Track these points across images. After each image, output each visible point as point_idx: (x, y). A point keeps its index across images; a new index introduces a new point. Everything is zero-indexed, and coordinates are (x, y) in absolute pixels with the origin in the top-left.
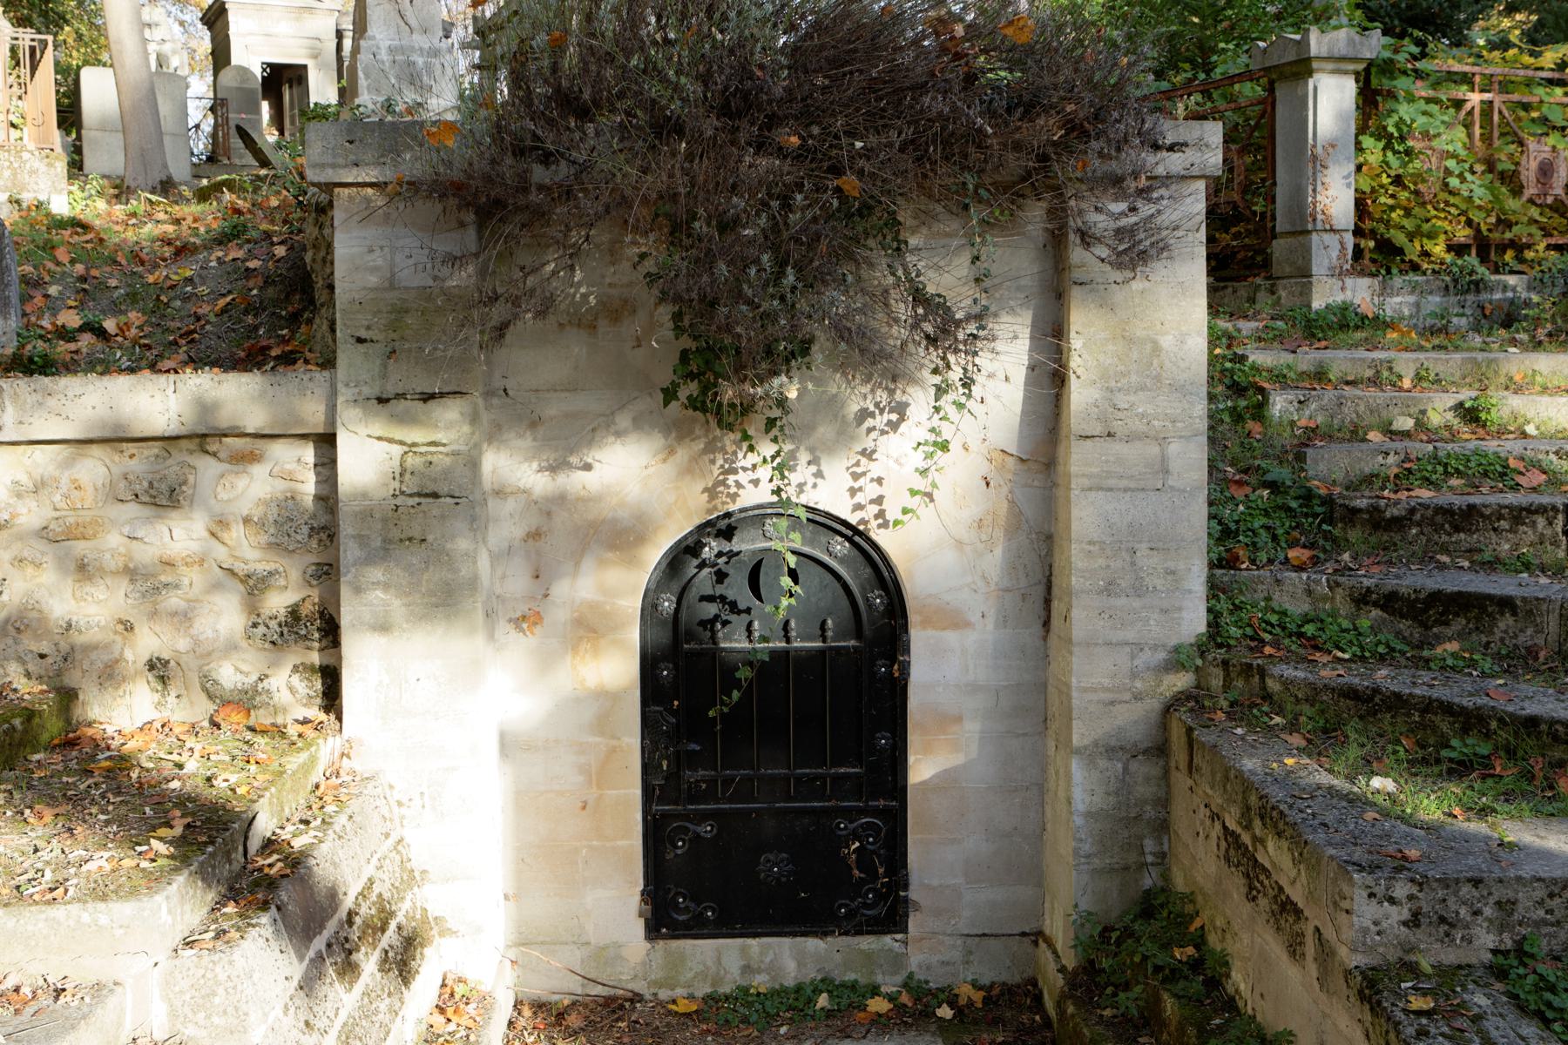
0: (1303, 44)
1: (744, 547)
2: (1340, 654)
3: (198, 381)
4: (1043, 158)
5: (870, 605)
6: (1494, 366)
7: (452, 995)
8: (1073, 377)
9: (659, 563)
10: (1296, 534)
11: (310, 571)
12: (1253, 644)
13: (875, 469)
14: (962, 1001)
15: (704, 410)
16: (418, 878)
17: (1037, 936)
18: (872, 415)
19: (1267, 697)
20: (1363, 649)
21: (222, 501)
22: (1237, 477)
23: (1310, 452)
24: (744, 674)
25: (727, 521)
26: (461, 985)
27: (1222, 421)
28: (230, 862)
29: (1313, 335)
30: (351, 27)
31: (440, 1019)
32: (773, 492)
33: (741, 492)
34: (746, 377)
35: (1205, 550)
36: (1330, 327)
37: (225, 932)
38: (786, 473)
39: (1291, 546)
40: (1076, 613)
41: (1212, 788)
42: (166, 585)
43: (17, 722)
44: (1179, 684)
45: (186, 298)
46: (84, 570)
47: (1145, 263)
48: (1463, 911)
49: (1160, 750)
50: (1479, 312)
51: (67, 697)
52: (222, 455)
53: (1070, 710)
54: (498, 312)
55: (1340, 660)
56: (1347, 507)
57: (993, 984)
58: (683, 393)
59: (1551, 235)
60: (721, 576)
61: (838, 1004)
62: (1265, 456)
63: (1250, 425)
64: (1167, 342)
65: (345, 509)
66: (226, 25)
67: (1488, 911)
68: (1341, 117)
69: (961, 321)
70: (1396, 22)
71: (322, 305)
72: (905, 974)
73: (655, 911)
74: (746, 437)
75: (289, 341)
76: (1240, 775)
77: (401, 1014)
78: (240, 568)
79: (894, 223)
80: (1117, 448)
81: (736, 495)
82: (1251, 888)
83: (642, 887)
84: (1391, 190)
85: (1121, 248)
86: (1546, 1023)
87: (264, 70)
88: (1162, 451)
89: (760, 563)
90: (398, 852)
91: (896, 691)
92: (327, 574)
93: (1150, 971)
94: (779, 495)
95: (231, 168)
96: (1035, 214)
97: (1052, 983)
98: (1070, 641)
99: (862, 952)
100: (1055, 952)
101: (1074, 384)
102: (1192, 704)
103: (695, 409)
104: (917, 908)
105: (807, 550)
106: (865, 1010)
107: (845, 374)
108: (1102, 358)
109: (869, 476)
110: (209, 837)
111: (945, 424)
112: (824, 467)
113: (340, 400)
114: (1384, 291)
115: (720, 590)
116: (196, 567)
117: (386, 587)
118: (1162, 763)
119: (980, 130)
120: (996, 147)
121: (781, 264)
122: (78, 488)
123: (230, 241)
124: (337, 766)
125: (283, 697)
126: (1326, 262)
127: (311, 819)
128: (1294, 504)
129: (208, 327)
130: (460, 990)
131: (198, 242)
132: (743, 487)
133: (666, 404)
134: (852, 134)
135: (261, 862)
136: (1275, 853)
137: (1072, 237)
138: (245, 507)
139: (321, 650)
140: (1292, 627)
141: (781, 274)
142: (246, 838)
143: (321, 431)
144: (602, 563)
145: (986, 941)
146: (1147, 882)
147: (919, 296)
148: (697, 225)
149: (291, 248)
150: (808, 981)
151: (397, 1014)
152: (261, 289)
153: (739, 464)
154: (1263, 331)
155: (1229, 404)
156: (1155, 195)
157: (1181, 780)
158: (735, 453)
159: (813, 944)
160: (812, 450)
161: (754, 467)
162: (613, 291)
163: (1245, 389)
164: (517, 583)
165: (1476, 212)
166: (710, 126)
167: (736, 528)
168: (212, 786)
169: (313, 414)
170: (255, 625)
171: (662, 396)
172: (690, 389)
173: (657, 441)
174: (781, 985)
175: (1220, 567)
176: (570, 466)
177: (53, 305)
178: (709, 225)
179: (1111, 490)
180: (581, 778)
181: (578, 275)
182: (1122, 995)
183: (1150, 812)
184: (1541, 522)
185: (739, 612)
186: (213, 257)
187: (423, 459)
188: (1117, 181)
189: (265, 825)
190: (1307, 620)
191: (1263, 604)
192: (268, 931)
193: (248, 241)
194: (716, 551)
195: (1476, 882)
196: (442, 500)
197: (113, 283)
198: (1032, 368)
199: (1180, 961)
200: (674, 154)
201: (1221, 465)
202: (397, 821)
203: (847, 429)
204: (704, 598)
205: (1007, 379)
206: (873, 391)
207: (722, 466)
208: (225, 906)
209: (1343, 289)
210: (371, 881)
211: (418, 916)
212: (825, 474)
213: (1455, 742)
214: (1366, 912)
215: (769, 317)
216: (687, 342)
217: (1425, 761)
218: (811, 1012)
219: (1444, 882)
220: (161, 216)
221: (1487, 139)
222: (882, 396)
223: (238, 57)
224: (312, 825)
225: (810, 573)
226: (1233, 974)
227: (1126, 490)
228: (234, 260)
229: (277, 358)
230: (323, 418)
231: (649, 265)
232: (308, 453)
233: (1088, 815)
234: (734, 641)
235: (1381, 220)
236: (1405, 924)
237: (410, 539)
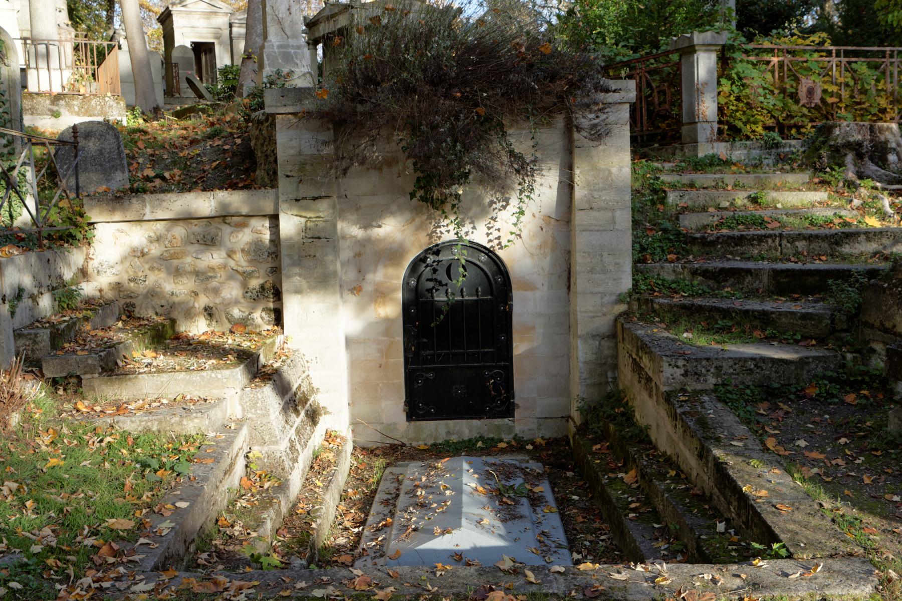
0: (691, 39)
1: (444, 258)
2: (684, 294)
3: (223, 194)
6: (768, 180)
8: (576, 185)
10: (672, 249)
13: (497, 225)
17: (568, 418)
18: (495, 203)
19: (654, 311)
20: (693, 292)
23: (681, 216)
29: (697, 169)
31: (327, 443)
36: (705, 165)
39: (669, 254)
40: (578, 281)
42: (211, 277)
43: (160, 327)
45: (198, 163)
46: (177, 273)
48: (703, 370)
49: (613, 336)
50: (778, 157)
51: (173, 322)
52: (232, 224)
54: (344, 164)
55: (683, 296)
56: (692, 237)
57: (550, 438)
58: (418, 195)
59: (815, 121)
60: (435, 271)
62: (664, 219)
63: (659, 206)
64: (614, 170)
66: (172, 23)
67: (712, 370)
68: (709, 72)
70: (763, 17)
72: (513, 434)
73: (410, 409)
74: (444, 212)
78: (240, 269)
79: (502, 126)
80: (594, 214)
81: (440, 237)
83: (404, 399)
84: (735, 103)
86: (726, 403)
89: (450, 265)
91: (507, 317)
92: (276, 271)
96: (560, 121)
98: (576, 293)
99: (496, 425)
101: (577, 188)
103: (423, 201)
104: (518, 407)
105: (469, 259)
107: (484, 187)
108: (587, 177)
109: (494, 228)
113: (280, 200)
114: (732, 148)
115: (434, 276)
116: (223, 269)
117: (300, 275)
118: (614, 341)
119: (533, 88)
121: (455, 142)
122: (175, 238)
123: (214, 137)
125: (259, 321)
126: (705, 136)
128: (671, 237)
130: (333, 434)
133: (411, 199)
134: (482, 91)
136: (645, 362)
139: (274, 302)
140: (667, 285)
141: (455, 146)
142: (258, 362)
143: (272, 213)
144: (385, 266)
145: (547, 420)
147: (512, 154)
148: (422, 127)
149: (243, 140)
150: (474, 437)
152: (231, 158)
156: (606, 111)
157: (621, 345)
158: (439, 220)
159: (476, 422)
161: (447, 225)
162: (388, 155)
163: (658, 191)
164: (350, 275)
165: (776, 112)
166: (427, 89)
169: (269, 209)
170: (247, 292)
172: (421, 193)
173: (408, 215)
176: (372, 226)
177: (141, 167)
178: (427, 127)
179: (592, 231)
180: (379, 354)
183: (610, 361)
184: (770, 241)
185: (443, 285)
186: (208, 145)
188: (587, 106)
190: (673, 282)
193: (223, 137)
195: (708, 359)
197: (165, 157)
198: (560, 182)
200: (413, 100)
201: (644, 222)
203: (484, 210)
204: (428, 280)
205: (550, 187)
206: (495, 193)
209: (712, 148)
210: (300, 386)
213: (719, 322)
214: (668, 371)
215: (450, 162)
217: (708, 330)
219: (696, 360)
220: (176, 126)
221: (781, 79)
222: (499, 195)
225: (472, 270)
227: (598, 231)
228: (218, 145)
230: (272, 208)
231: (404, 143)
232: (267, 223)
233: (585, 362)
234: (440, 297)
235: (731, 116)
236: (682, 375)
237: (309, 256)
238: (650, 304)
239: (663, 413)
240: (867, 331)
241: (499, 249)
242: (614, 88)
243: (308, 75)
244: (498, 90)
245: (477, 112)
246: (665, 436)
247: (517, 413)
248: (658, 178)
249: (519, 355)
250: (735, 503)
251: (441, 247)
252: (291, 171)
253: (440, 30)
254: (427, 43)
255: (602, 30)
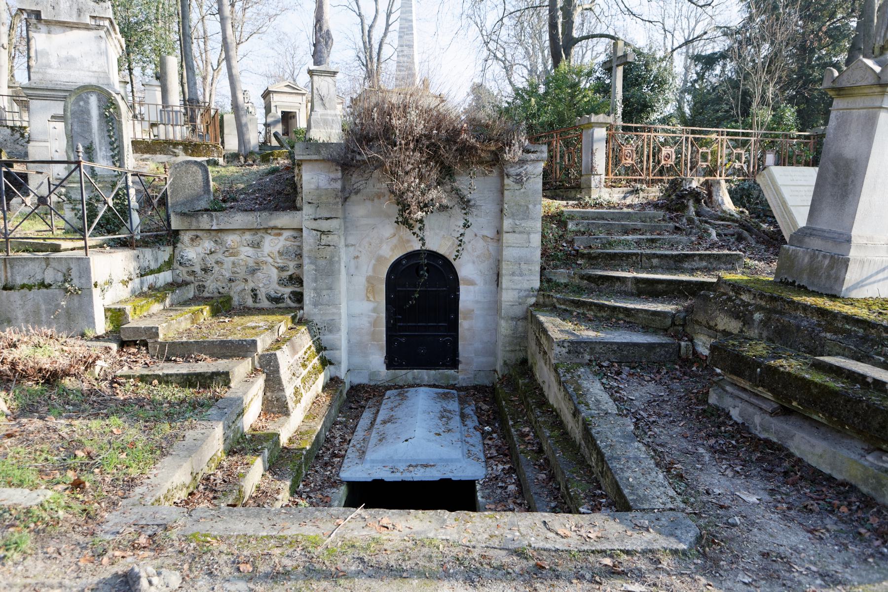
17: (495, 371)
48: (582, 350)
67: (588, 350)
159: (433, 372)
184: (634, 258)
239: (553, 379)
240: (697, 327)
246: (553, 394)
247: (460, 367)
250: (595, 456)
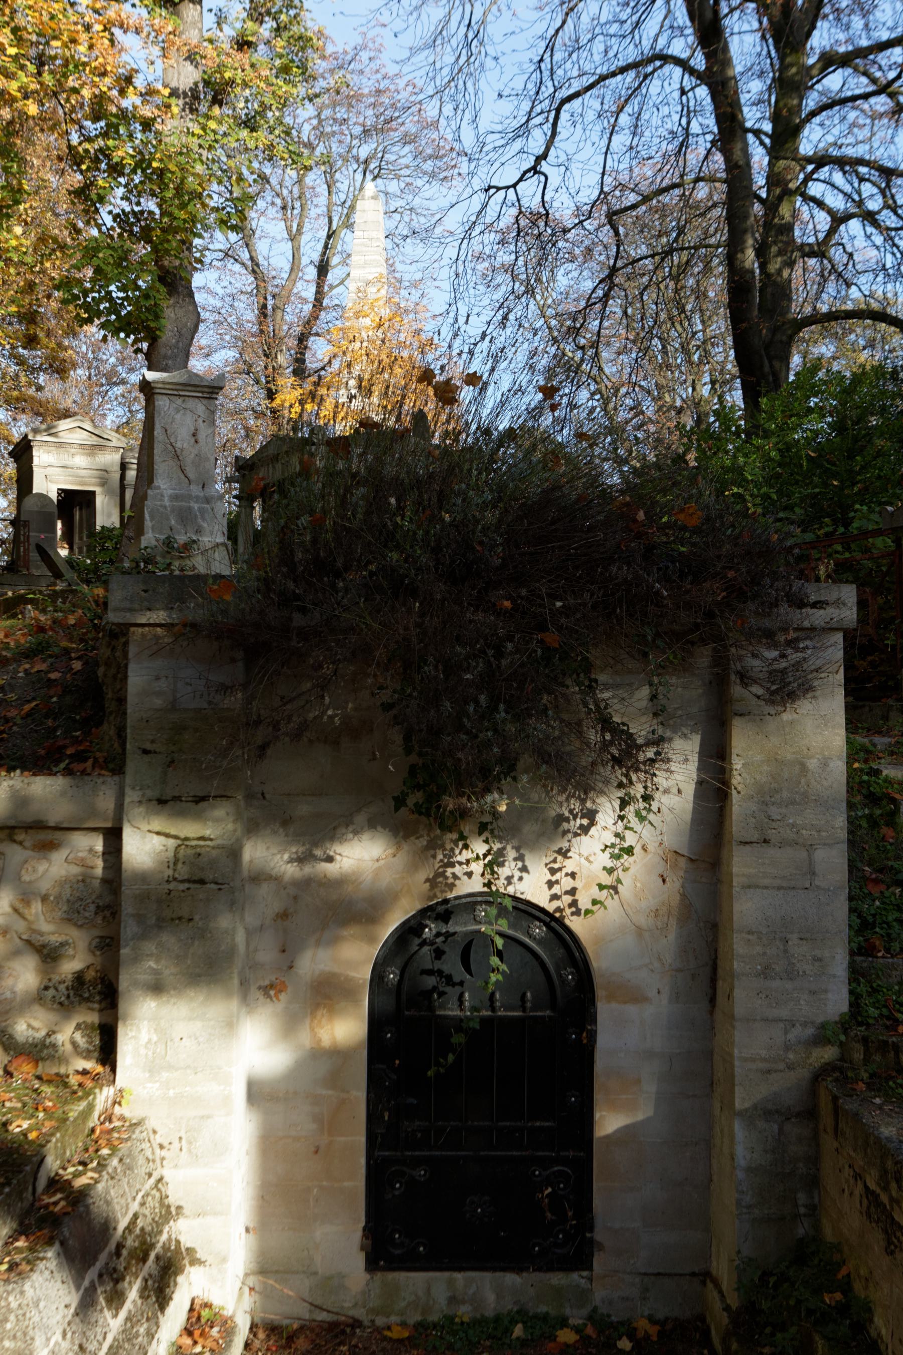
1: (459, 929)
4: (710, 615)
5: (563, 981)
7: (199, 1318)
8: (734, 792)
9: (386, 941)
11: (94, 943)
12: (888, 1023)
13: (570, 865)
14: (640, 1334)
15: (428, 815)
16: (174, 1213)
17: (706, 1276)
18: (567, 820)
21: (25, 882)
22: (874, 876)
24: (458, 1039)
25: (444, 907)
26: (207, 1310)
27: (860, 826)
28: (21, 1200)
30: (135, 461)
31: (188, 1341)
32: (485, 885)
33: (457, 882)
34: (464, 793)
35: (846, 942)
37: (17, 1265)
38: (496, 869)
40: (737, 993)
41: (855, 1150)
44: (826, 1056)
47: (794, 701)
49: (810, 1114)
53: (733, 1076)
58: (411, 801)
60: (439, 954)
61: (532, 1334)
63: (885, 830)
65: (127, 892)
69: (642, 746)
71: (111, 713)
75: (81, 741)
76: (878, 1140)
77: (156, 1337)
78: (38, 940)
79: (587, 667)
82: (889, 1242)
83: (363, 1224)
85: (774, 687)
87: (59, 494)
88: (809, 856)
89: (470, 943)
90: (159, 1190)
93: (803, 1314)
94: (489, 887)
95: (31, 580)
96: (703, 658)
97: (719, 1320)
98: (732, 1017)
100: (721, 1292)
102: (837, 1074)
103: (420, 814)
104: (601, 1247)
105: (511, 932)
106: (555, 1340)
109: (564, 871)
110: (6, 1178)
111: (628, 834)
112: (527, 863)
113: (127, 800)
115: (437, 965)
119: (658, 593)
120: (671, 606)
123: (36, 655)
124: (109, 1112)
127: (88, 1161)
129: (15, 728)
130: (205, 1313)
131: (9, 655)
132: (459, 878)
133: (397, 809)
134: (554, 597)
135: (47, 1200)
137: (733, 677)
138: (45, 886)
146: (801, 1232)
149: (86, 664)
151: (153, 1338)
152: (59, 697)
153: (455, 859)
154: (895, 746)
155: (867, 811)
157: (828, 1142)
158: (452, 850)
159: (511, 1279)
160: (517, 849)
161: (468, 862)
163: (880, 799)
164: (267, 954)
167: (452, 913)
168: (7, 1131)
170: (46, 988)
171: (393, 803)
174: (482, 1316)
175: (860, 954)
179: (766, 888)
181: (327, 700)
182: (779, 1336)
185: (454, 985)
186: (21, 669)
187: (193, 851)
189: (52, 1163)
191: (896, 987)
192: (52, 1264)
193: (51, 656)
194: (434, 932)
196: (208, 886)
198: (700, 783)
199: (829, 1306)
201: (859, 865)
202: (158, 1161)
205: (679, 792)
206: (567, 800)
207: (441, 861)
208: (17, 1240)
210: (136, 1216)
211: (173, 1247)
212: (529, 868)
216: (414, 758)
218: (508, 1341)
222: (576, 805)
223: (39, 486)
224: (90, 1166)
226: (876, 1319)
228: (38, 672)
229: (71, 756)
233: (749, 1170)
238: (892, 1054)
241: (573, 914)
242: (813, 598)
243: (222, 548)
244: (587, 596)
245: (542, 642)
247: (598, 1262)
248: (878, 772)
249: (608, 1137)
251: (454, 906)
252: (153, 742)
253: (469, 471)
254: (442, 497)
255: (741, 491)
